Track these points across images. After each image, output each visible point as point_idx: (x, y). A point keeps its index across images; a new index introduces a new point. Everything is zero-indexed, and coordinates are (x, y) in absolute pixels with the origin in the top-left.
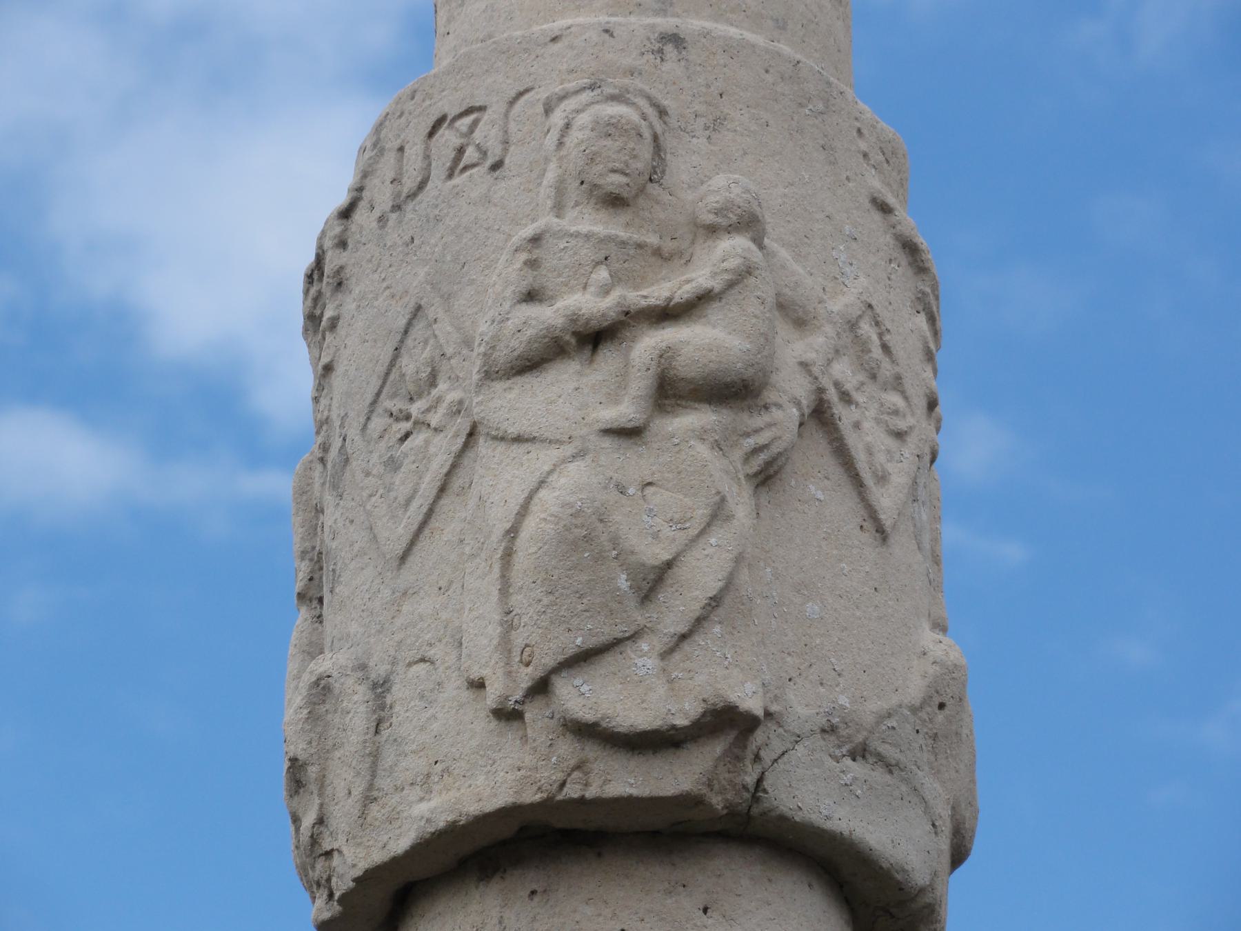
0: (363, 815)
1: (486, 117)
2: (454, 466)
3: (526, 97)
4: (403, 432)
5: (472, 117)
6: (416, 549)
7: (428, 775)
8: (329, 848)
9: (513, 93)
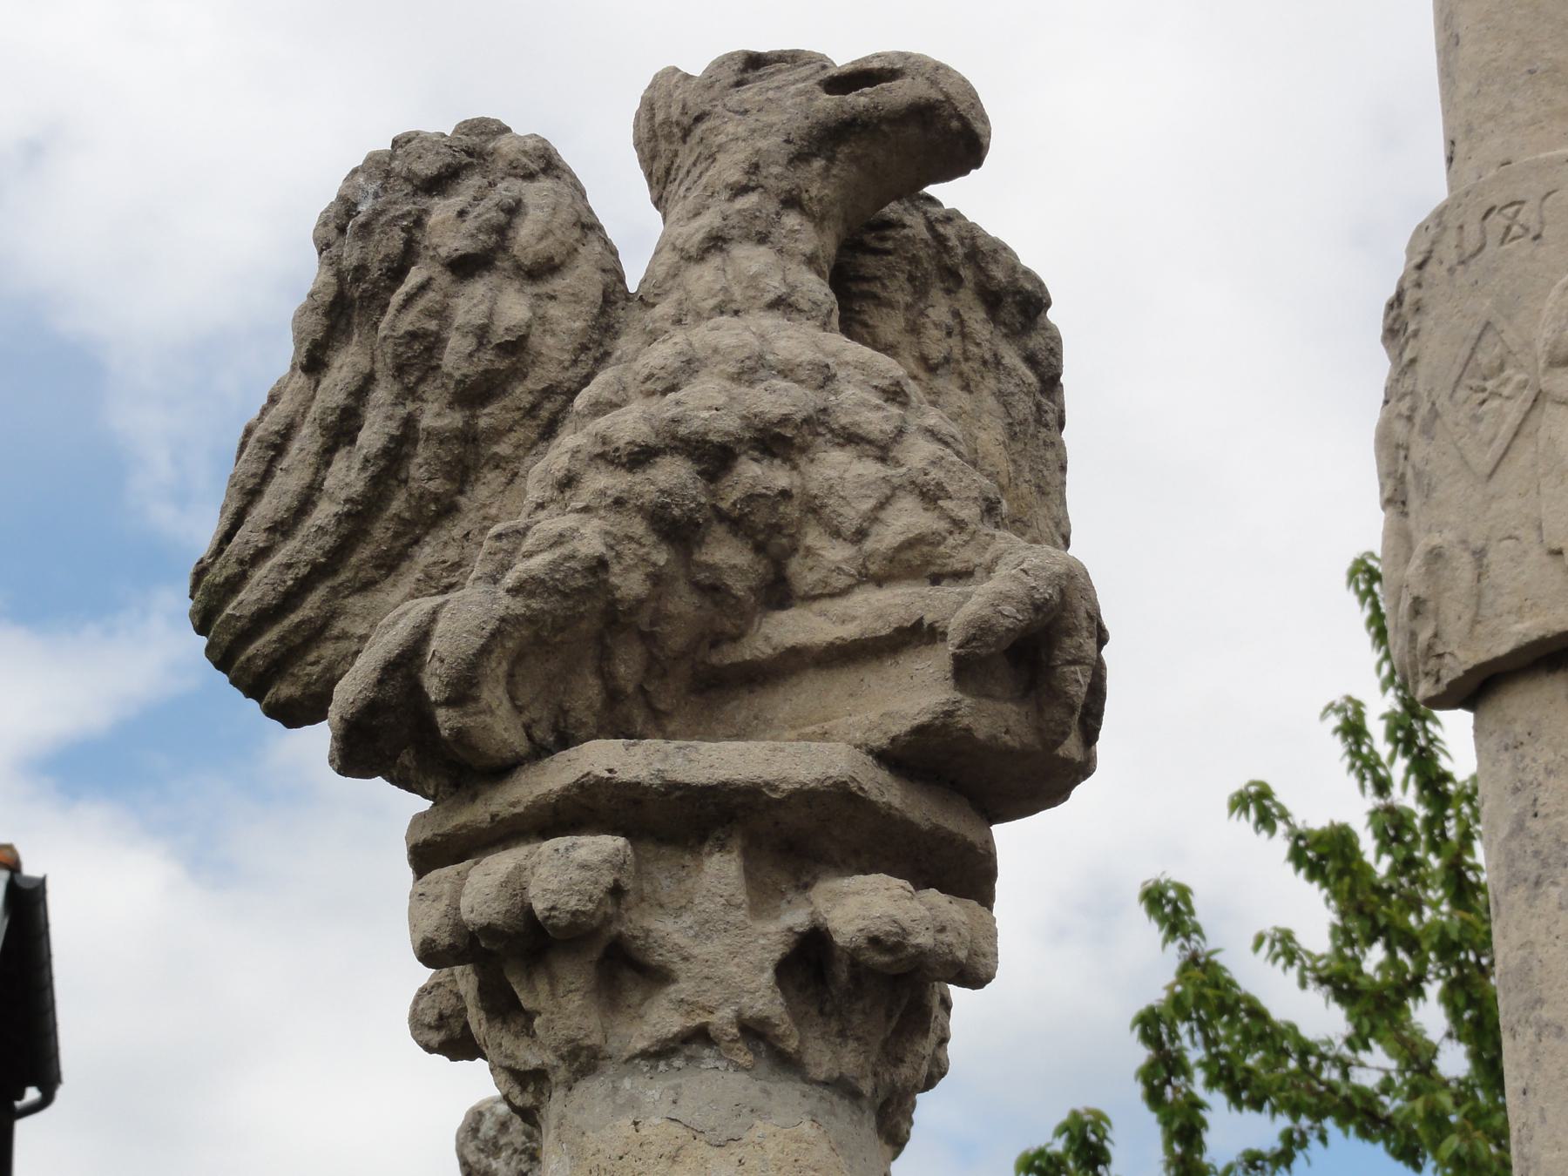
0: (1471, 631)
1: (1525, 208)
2: (1524, 420)
3: (1554, 195)
4: (1481, 399)
5: (1515, 208)
6: (1499, 471)
7: (1520, 608)
8: (1441, 652)
9: (1544, 193)
